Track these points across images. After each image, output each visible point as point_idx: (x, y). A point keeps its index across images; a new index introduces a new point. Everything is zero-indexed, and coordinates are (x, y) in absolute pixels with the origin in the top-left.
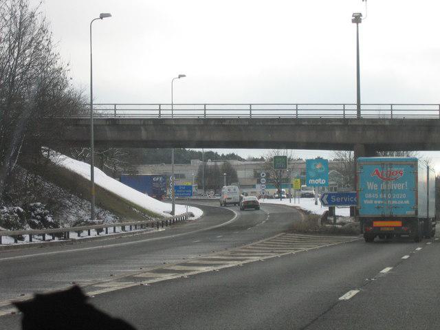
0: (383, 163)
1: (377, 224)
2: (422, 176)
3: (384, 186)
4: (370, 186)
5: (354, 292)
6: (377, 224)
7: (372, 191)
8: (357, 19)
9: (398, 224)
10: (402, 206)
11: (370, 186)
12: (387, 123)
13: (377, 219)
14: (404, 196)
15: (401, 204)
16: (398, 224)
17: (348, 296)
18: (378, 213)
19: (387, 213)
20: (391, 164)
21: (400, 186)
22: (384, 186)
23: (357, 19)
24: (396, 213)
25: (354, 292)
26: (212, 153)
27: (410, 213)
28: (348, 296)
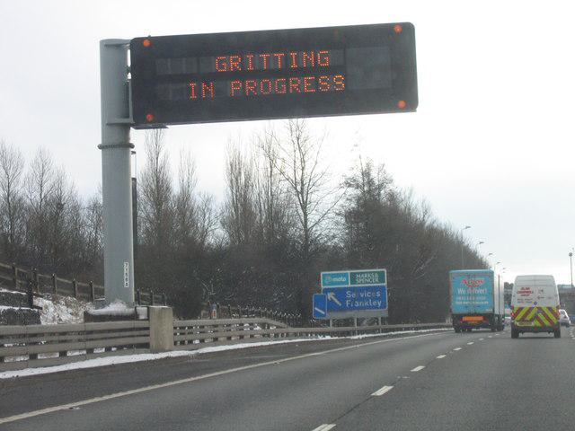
0: (469, 275)
1: (465, 319)
2: (496, 280)
3: (470, 291)
4: (461, 291)
5: (415, 370)
6: (465, 319)
7: (460, 295)
8: (571, 255)
9: (481, 318)
10: (484, 306)
11: (461, 291)
12: (149, 117)
13: (465, 315)
14: (485, 298)
15: (482, 305)
16: (481, 318)
17: (381, 392)
18: (465, 311)
19: (472, 311)
20: (474, 275)
21: (481, 291)
22: (470, 291)
23: (571, 255)
24: (479, 311)
25: (415, 370)
26: (10, 289)
27: (489, 310)
28: (381, 392)
